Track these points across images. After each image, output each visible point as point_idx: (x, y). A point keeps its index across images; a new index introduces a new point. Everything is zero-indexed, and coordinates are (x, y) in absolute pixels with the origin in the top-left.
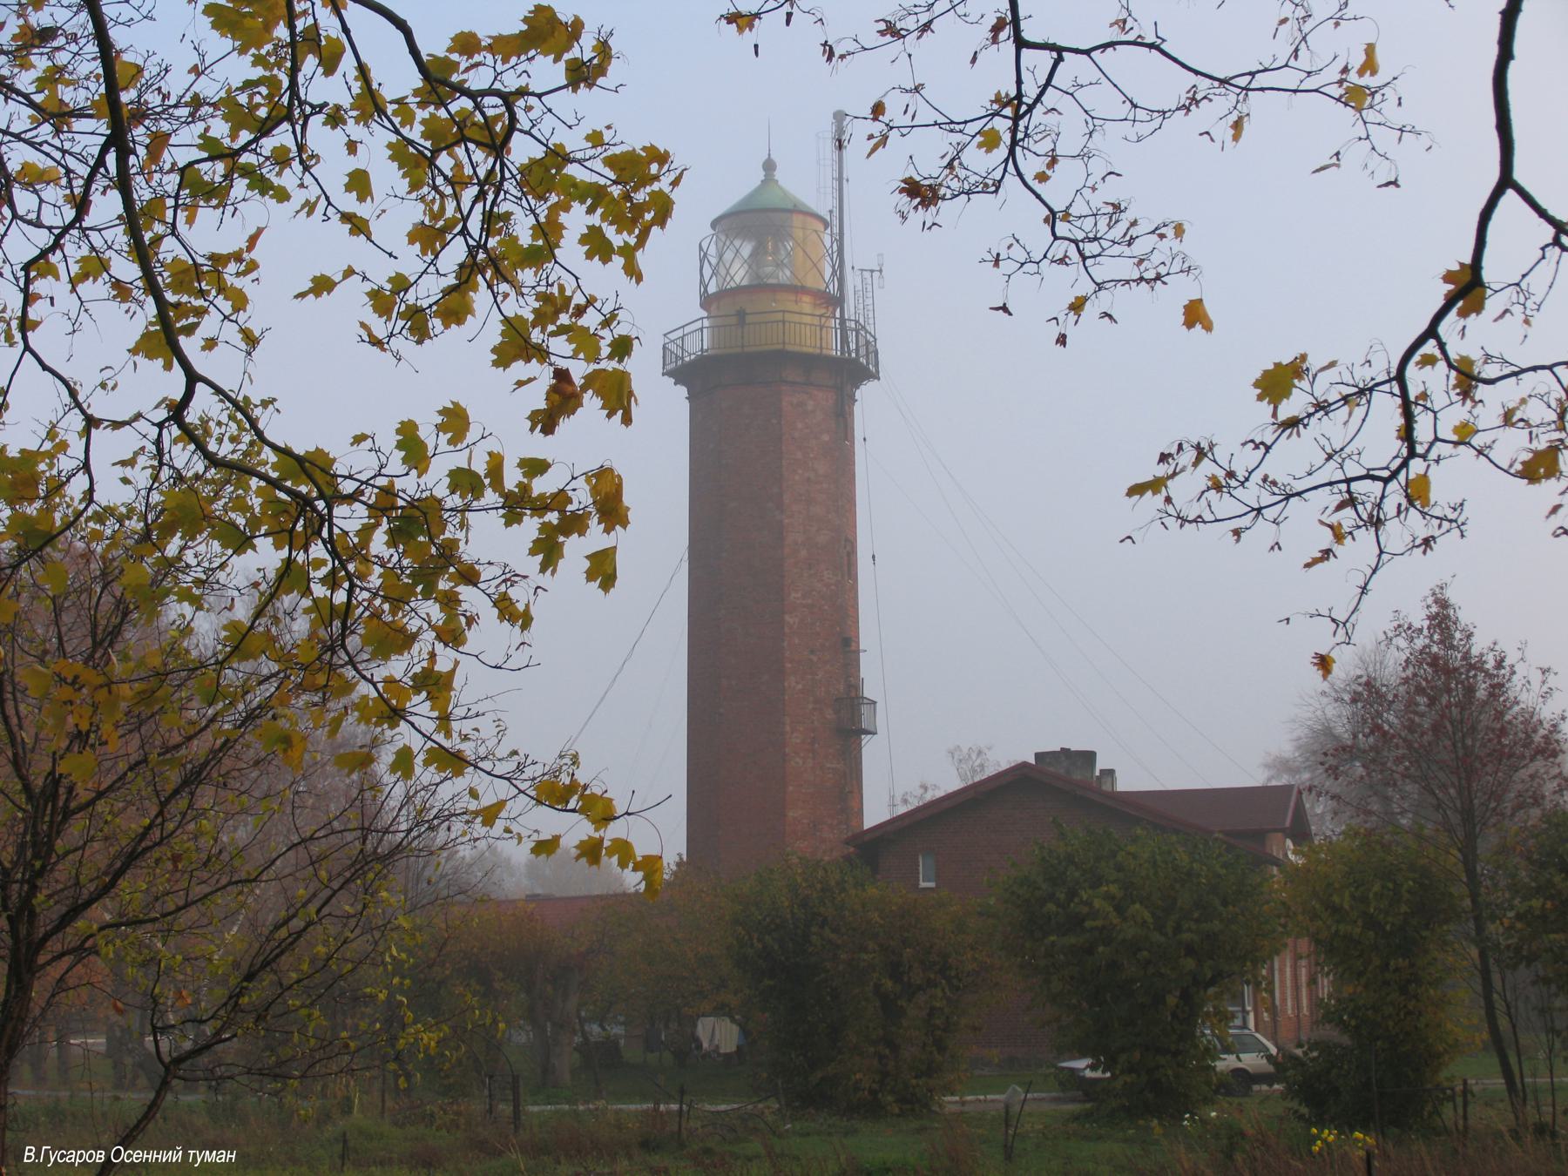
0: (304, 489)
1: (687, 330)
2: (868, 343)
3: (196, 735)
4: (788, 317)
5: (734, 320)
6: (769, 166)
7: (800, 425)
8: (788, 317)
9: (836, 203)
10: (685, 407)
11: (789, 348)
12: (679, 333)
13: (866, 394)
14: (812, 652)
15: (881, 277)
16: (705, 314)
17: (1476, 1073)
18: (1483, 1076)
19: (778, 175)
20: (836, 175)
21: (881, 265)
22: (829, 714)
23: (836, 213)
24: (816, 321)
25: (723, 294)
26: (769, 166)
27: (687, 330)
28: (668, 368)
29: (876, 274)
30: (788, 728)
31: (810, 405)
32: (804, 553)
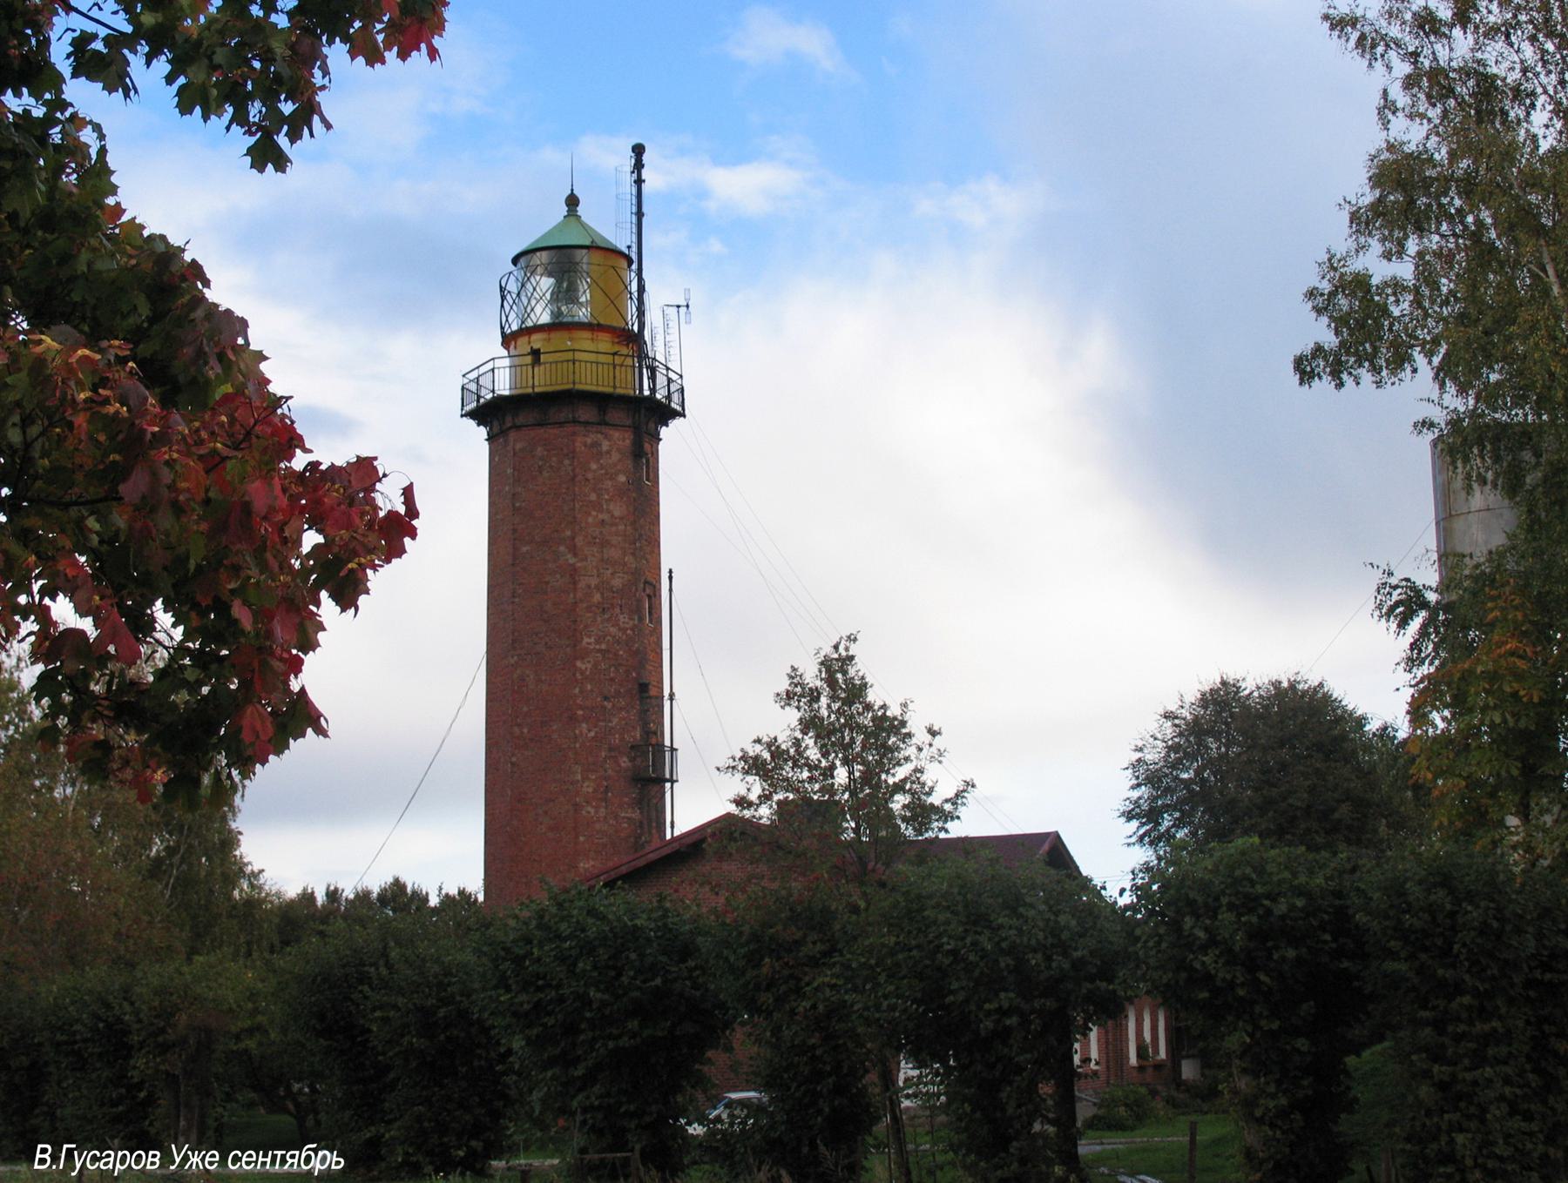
0: (1548, 976)
1: (482, 370)
2: (670, 381)
3: (100, 500)
4: (578, 356)
5: (529, 359)
6: (572, 201)
7: (594, 466)
8: (578, 356)
9: (634, 239)
10: (485, 448)
11: (579, 387)
12: (489, 366)
13: (670, 434)
14: (606, 698)
15: (688, 313)
16: (505, 353)
17: (1442, 1170)
18: (1442, 1170)
19: (581, 210)
20: (634, 209)
21: (687, 300)
22: (624, 762)
23: (634, 249)
24: (609, 359)
25: (525, 331)
26: (572, 201)
27: (482, 370)
28: (468, 408)
29: (683, 310)
30: (579, 777)
31: (605, 445)
32: (597, 597)
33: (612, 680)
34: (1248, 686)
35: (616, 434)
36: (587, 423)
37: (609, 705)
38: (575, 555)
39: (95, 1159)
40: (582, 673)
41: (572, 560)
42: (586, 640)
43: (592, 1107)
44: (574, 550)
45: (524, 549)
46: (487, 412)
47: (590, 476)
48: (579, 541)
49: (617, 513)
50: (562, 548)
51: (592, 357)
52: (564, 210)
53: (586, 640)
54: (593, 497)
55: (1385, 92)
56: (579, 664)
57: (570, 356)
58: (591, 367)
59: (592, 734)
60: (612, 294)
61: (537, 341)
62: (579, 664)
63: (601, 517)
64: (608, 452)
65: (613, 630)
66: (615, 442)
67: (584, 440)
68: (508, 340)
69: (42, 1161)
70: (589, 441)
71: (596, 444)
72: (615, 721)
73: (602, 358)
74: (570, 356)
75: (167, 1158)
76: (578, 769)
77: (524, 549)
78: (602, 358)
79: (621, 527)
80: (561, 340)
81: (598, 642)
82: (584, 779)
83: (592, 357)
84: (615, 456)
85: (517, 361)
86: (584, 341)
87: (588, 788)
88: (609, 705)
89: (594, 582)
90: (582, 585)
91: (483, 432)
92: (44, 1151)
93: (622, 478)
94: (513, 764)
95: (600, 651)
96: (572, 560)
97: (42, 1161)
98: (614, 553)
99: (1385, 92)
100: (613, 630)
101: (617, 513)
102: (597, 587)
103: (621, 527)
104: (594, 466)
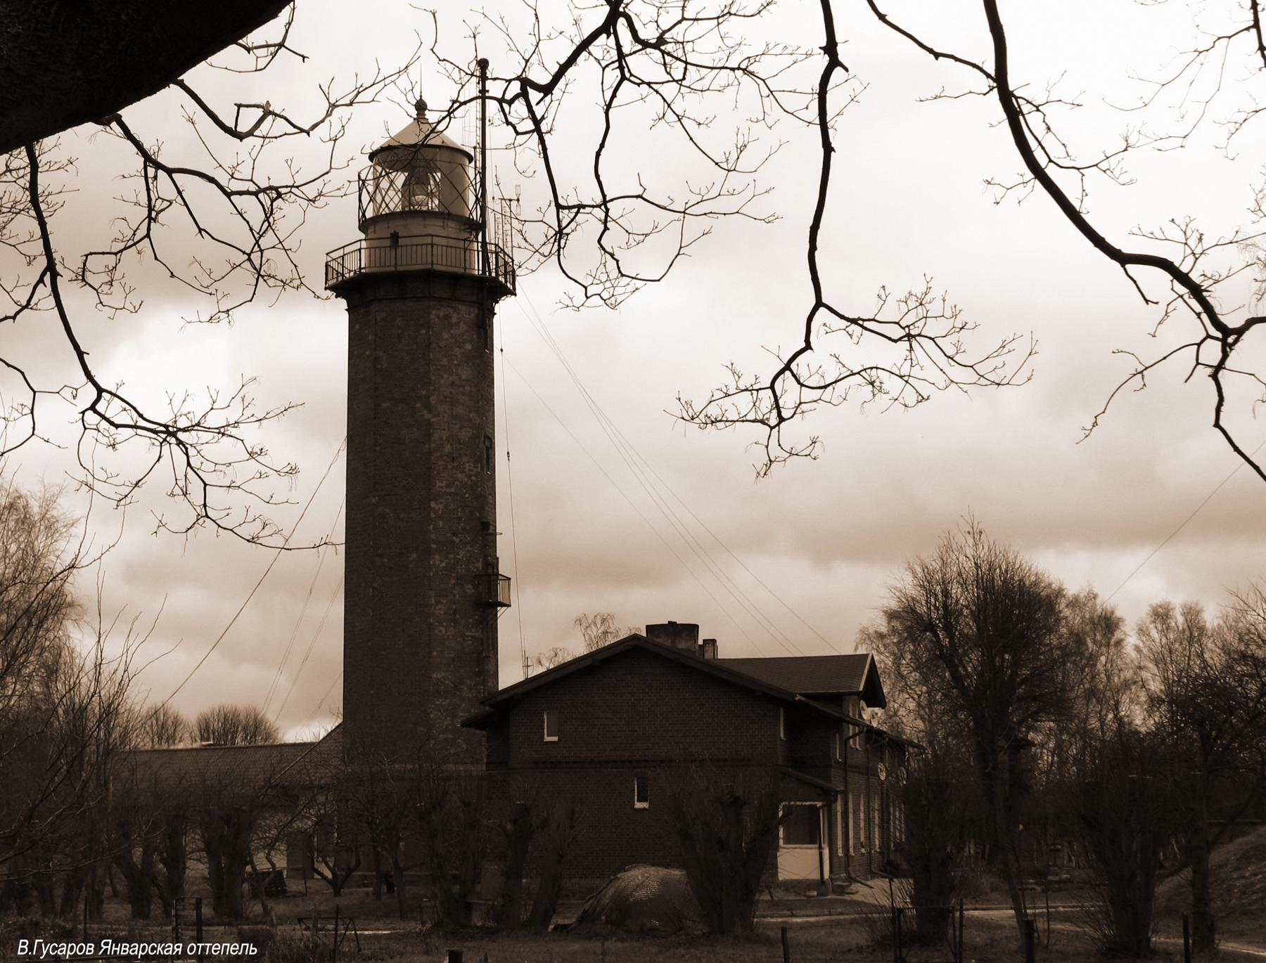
1: (347, 250)
4: (436, 240)
5: (388, 243)
7: (445, 335)
8: (436, 240)
10: (345, 317)
13: (504, 309)
14: (455, 534)
16: (363, 236)
20: (480, 115)
22: (469, 589)
25: (378, 218)
27: (347, 250)
28: (330, 283)
29: (514, 203)
31: (454, 319)
32: (448, 448)
33: (460, 519)
34: (80, 641)
35: (463, 309)
36: (439, 299)
37: (457, 540)
38: (430, 412)
39: (55, 949)
40: (436, 513)
41: (427, 416)
42: (439, 484)
43: (175, 929)
44: (428, 407)
45: (385, 405)
46: (345, 287)
47: (442, 344)
48: (433, 399)
49: (464, 377)
50: (419, 405)
51: (443, 241)
52: (414, 113)
53: (439, 484)
54: (445, 362)
55: (847, 70)
56: (433, 504)
57: (428, 240)
58: (430, 250)
59: (444, 565)
60: (454, 186)
61: (396, 226)
62: (433, 504)
63: (451, 379)
64: (457, 324)
65: (460, 475)
66: (466, 313)
67: (436, 314)
68: (365, 225)
69: (23, 950)
70: (442, 314)
71: (447, 317)
72: (462, 553)
73: (452, 243)
74: (428, 240)
75: (98, 948)
76: (432, 593)
77: (385, 405)
78: (452, 243)
79: (467, 388)
80: (416, 227)
81: (448, 486)
82: (438, 602)
83: (443, 241)
84: (463, 327)
85: (375, 243)
86: (435, 227)
87: (440, 610)
88: (457, 540)
89: (445, 435)
90: (436, 436)
91: (343, 303)
92: (24, 944)
93: (468, 346)
94: (374, 589)
95: (450, 494)
96: (427, 416)
97: (23, 950)
98: (460, 410)
99: (847, 70)
100: (460, 475)
101: (464, 377)
102: (448, 440)
103: (467, 388)
104: (445, 335)
